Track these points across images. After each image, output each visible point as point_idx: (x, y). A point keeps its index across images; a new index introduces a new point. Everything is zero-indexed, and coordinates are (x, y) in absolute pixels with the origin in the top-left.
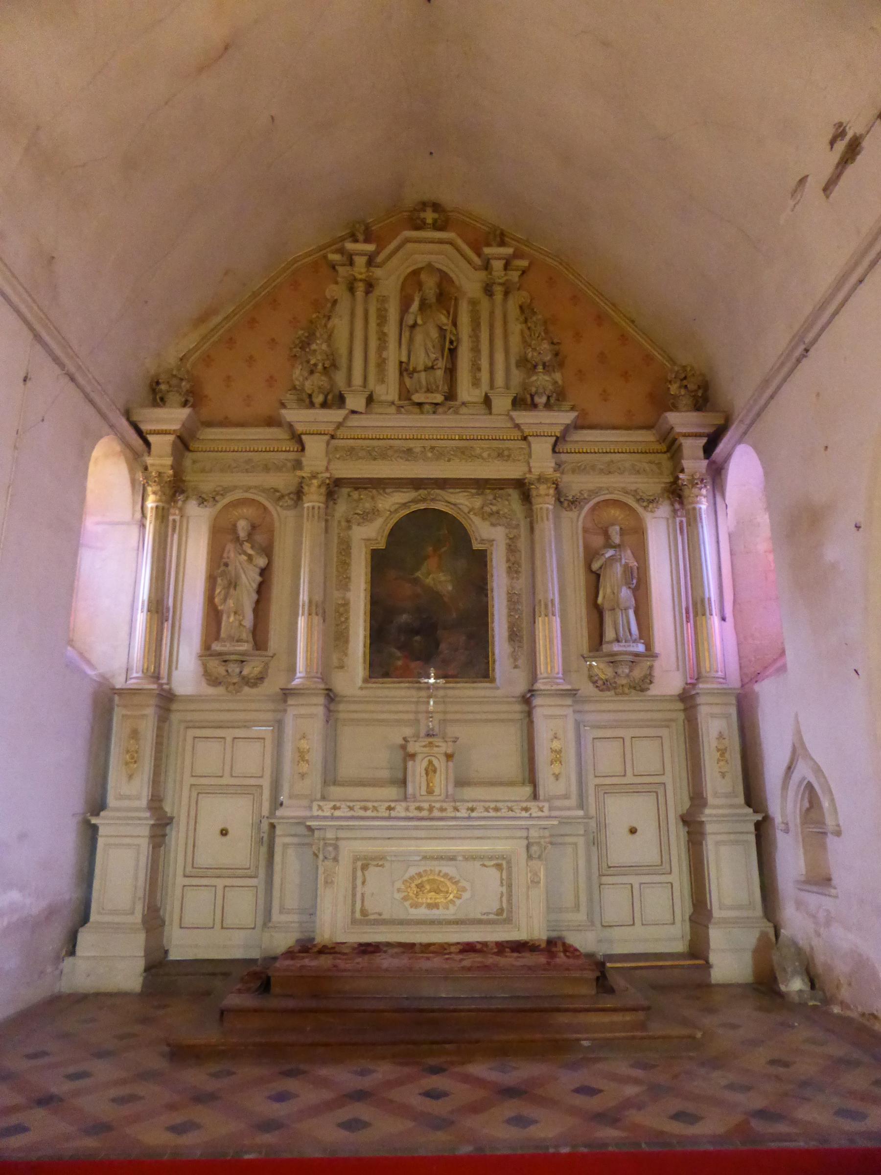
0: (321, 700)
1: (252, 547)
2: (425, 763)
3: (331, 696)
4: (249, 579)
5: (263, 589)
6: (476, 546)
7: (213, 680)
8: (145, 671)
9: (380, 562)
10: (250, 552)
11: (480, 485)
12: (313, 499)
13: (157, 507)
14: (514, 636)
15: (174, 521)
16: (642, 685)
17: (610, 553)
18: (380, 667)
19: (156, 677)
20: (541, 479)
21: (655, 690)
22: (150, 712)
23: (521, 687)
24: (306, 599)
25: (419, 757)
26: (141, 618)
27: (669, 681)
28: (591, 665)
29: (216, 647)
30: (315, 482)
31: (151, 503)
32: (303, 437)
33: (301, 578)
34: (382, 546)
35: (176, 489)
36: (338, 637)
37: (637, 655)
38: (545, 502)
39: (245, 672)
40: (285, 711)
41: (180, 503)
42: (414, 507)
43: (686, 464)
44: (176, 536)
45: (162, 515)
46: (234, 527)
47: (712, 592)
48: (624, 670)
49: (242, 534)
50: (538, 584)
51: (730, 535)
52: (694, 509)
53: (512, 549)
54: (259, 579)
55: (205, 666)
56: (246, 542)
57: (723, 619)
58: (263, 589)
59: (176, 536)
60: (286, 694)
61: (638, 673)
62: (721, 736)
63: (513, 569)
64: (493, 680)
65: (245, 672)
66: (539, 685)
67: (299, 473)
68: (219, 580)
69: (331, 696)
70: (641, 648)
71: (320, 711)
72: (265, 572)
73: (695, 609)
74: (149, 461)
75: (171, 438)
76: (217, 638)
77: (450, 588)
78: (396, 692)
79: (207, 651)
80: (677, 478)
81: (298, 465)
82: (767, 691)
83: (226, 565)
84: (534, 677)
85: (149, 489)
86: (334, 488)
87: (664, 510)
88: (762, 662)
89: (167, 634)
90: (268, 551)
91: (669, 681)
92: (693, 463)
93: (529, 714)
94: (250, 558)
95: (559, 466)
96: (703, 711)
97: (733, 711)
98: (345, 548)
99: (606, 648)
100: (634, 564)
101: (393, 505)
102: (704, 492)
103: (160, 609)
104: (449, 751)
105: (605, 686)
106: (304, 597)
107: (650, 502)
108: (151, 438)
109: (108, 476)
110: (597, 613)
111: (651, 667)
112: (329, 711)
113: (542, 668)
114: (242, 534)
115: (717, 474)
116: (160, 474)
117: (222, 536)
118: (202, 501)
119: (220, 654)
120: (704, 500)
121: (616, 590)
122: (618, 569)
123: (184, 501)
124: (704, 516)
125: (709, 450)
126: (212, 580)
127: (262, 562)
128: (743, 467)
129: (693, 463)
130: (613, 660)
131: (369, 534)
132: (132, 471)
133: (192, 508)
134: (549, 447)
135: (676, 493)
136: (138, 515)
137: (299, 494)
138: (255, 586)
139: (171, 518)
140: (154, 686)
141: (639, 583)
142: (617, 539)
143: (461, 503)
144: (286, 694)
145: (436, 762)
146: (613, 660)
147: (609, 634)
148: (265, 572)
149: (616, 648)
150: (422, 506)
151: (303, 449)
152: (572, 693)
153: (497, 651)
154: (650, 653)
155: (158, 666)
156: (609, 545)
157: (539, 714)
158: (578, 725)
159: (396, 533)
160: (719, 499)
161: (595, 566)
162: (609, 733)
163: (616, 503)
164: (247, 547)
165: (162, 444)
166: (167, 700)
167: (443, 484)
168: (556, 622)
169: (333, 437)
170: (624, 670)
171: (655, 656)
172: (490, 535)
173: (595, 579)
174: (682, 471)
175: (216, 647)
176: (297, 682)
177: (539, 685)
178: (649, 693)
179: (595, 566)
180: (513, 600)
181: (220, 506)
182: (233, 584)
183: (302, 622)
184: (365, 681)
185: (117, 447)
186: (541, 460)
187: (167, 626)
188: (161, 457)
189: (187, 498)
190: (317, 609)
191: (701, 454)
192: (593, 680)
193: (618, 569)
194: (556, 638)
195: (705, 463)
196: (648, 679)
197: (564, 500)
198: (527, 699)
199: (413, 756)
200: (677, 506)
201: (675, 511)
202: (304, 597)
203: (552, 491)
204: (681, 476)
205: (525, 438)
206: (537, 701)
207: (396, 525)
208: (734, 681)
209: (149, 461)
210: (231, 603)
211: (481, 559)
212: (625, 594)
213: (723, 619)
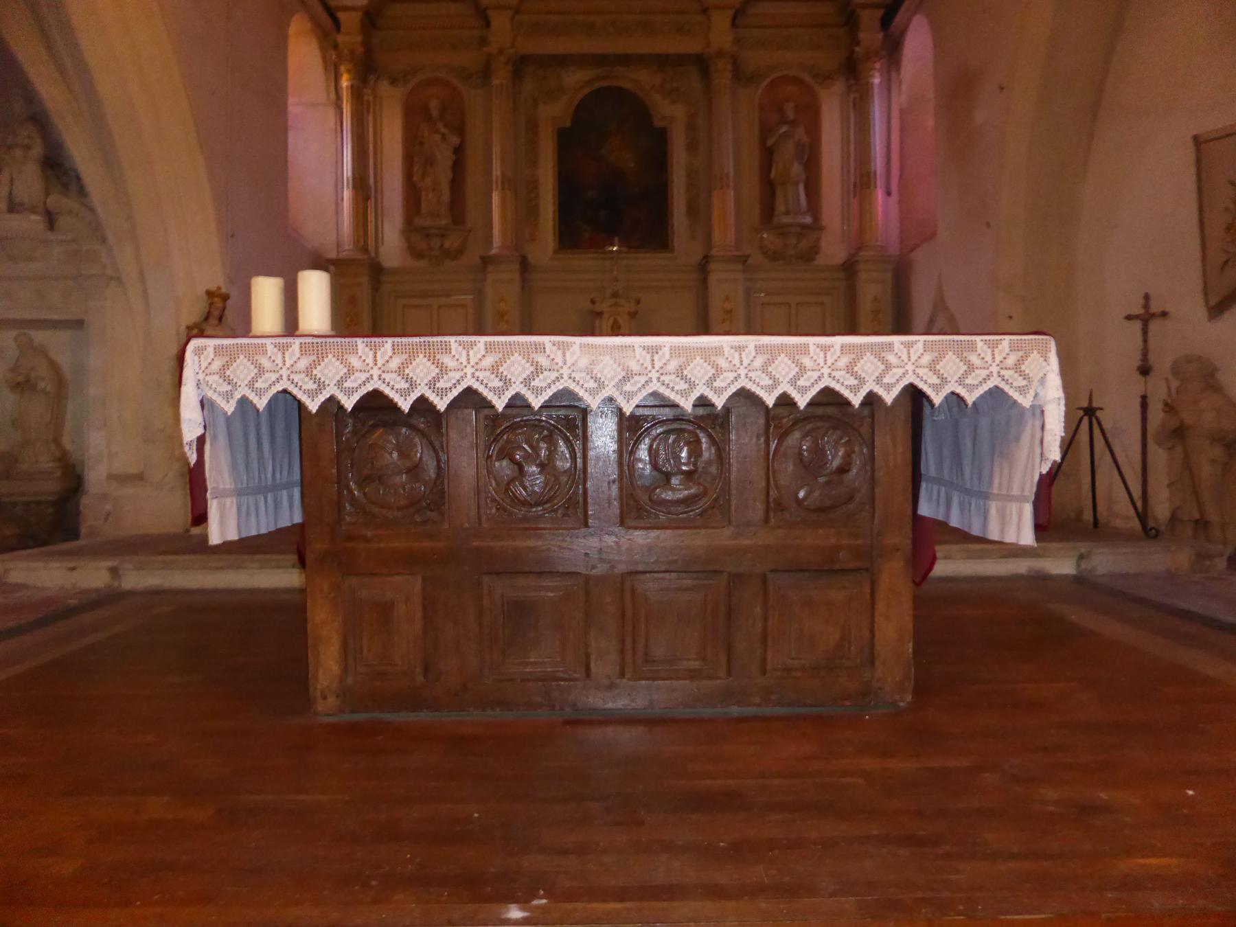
0: (516, 267)
1: (446, 126)
2: (611, 321)
3: (525, 266)
4: (444, 157)
5: (458, 166)
6: (658, 123)
7: (413, 251)
8: (356, 242)
9: (566, 140)
10: (443, 130)
11: (663, 62)
12: (500, 78)
13: (352, 86)
14: (692, 210)
15: (368, 101)
16: (809, 255)
17: (784, 129)
18: (568, 238)
19: (365, 250)
20: (720, 54)
21: (820, 261)
22: (365, 280)
23: (698, 257)
24: (499, 173)
25: (605, 316)
26: (347, 194)
27: (833, 250)
28: (762, 238)
29: (418, 222)
30: (502, 58)
31: (345, 83)
32: (490, 13)
33: (494, 156)
34: (568, 124)
35: (368, 69)
36: (527, 211)
37: (804, 226)
38: (723, 76)
39: (446, 245)
40: (485, 280)
41: (372, 83)
42: (597, 85)
43: (863, 36)
44: (371, 118)
45: (357, 94)
46: (426, 108)
47: (878, 165)
48: (793, 241)
49: (435, 113)
50: (714, 160)
51: (902, 111)
52: (868, 83)
53: (691, 126)
54: (454, 157)
55: (408, 240)
56: (437, 124)
57: (889, 194)
58: (458, 166)
59: (371, 118)
60: (486, 261)
61: (805, 244)
62: (876, 299)
63: (692, 147)
64: (672, 251)
65: (446, 245)
66: (714, 252)
67: (485, 49)
68: (416, 159)
69: (525, 266)
70: (808, 220)
71: (517, 276)
72: (459, 151)
73: (861, 183)
74: (341, 39)
75: (359, 14)
76: (418, 213)
77: (632, 165)
78: (585, 263)
79: (410, 227)
80: (852, 52)
81: (484, 41)
82: (920, 256)
83: (422, 143)
84: (709, 245)
85: (342, 68)
86: (520, 64)
87: (839, 86)
88: (918, 233)
89: (371, 217)
90: (460, 130)
91: (833, 250)
92: (870, 36)
93: (704, 281)
94: (444, 137)
95: (737, 41)
96: (863, 276)
97: (889, 276)
98: (533, 127)
99: (776, 220)
100: (805, 139)
101: (574, 78)
102: (877, 66)
103: (364, 188)
104: (633, 310)
105: (775, 256)
106: (497, 172)
107: (825, 78)
108: (341, 16)
109: (304, 56)
110: (769, 188)
111: (818, 240)
112: (524, 279)
113: (717, 237)
114: (435, 113)
115: (892, 49)
116: (352, 52)
117: (415, 116)
118: (394, 81)
119: (423, 228)
120: (877, 74)
121: (789, 164)
122: (790, 147)
123: (376, 81)
124: (876, 90)
125: (885, 23)
126: (408, 160)
127: (455, 140)
128: (918, 42)
129: (870, 36)
130: (782, 232)
131: (554, 113)
132: (323, 50)
133: (384, 88)
134: (728, 21)
135: (852, 70)
136: (333, 96)
137: (486, 73)
138: (450, 163)
139: (366, 98)
140: (365, 257)
141: (811, 160)
142: (791, 115)
143: (641, 80)
144: (486, 261)
145: (621, 322)
146: (782, 232)
147: (780, 207)
148: (459, 151)
149: (786, 220)
150: (605, 84)
151: (488, 25)
152: (744, 260)
153: (676, 224)
154: (817, 226)
155: (366, 241)
156: (783, 121)
157: (713, 278)
158: (748, 293)
159: (583, 110)
160: (894, 75)
161: (770, 143)
162: (777, 299)
163: (795, 80)
164: (440, 126)
165: (350, 20)
166: (377, 270)
167: (626, 60)
168: (731, 194)
169: (517, 12)
170: (793, 241)
171: (821, 228)
172: (670, 113)
173: (768, 155)
174: (858, 44)
175: (418, 222)
176: (493, 252)
177: (714, 252)
178: (816, 263)
179: (770, 143)
180: (691, 176)
181: (410, 86)
182: (430, 162)
183: (496, 197)
184: (555, 252)
185: (308, 25)
186: (721, 34)
187: (371, 203)
188: (351, 37)
189: (378, 78)
190: (509, 184)
191: (878, 24)
192: (764, 251)
193: (790, 147)
194: (730, 210)
195: (881, 36)
196: (814, 251)
197: (741, 76)
198: (703, 267)
199: (600, 314)
200: (852, 82)
201: (849, 88)
202: (497, 172)
203: (729, 67)
204: (857, 49)
205: (705, 11)
206: (713, 266)
207: (579, 105)
208: (894, 250)
209: (341, 39)
210: (428, 180)
211: (661, 137)
212: (797, 169)
213: (889, 194)
